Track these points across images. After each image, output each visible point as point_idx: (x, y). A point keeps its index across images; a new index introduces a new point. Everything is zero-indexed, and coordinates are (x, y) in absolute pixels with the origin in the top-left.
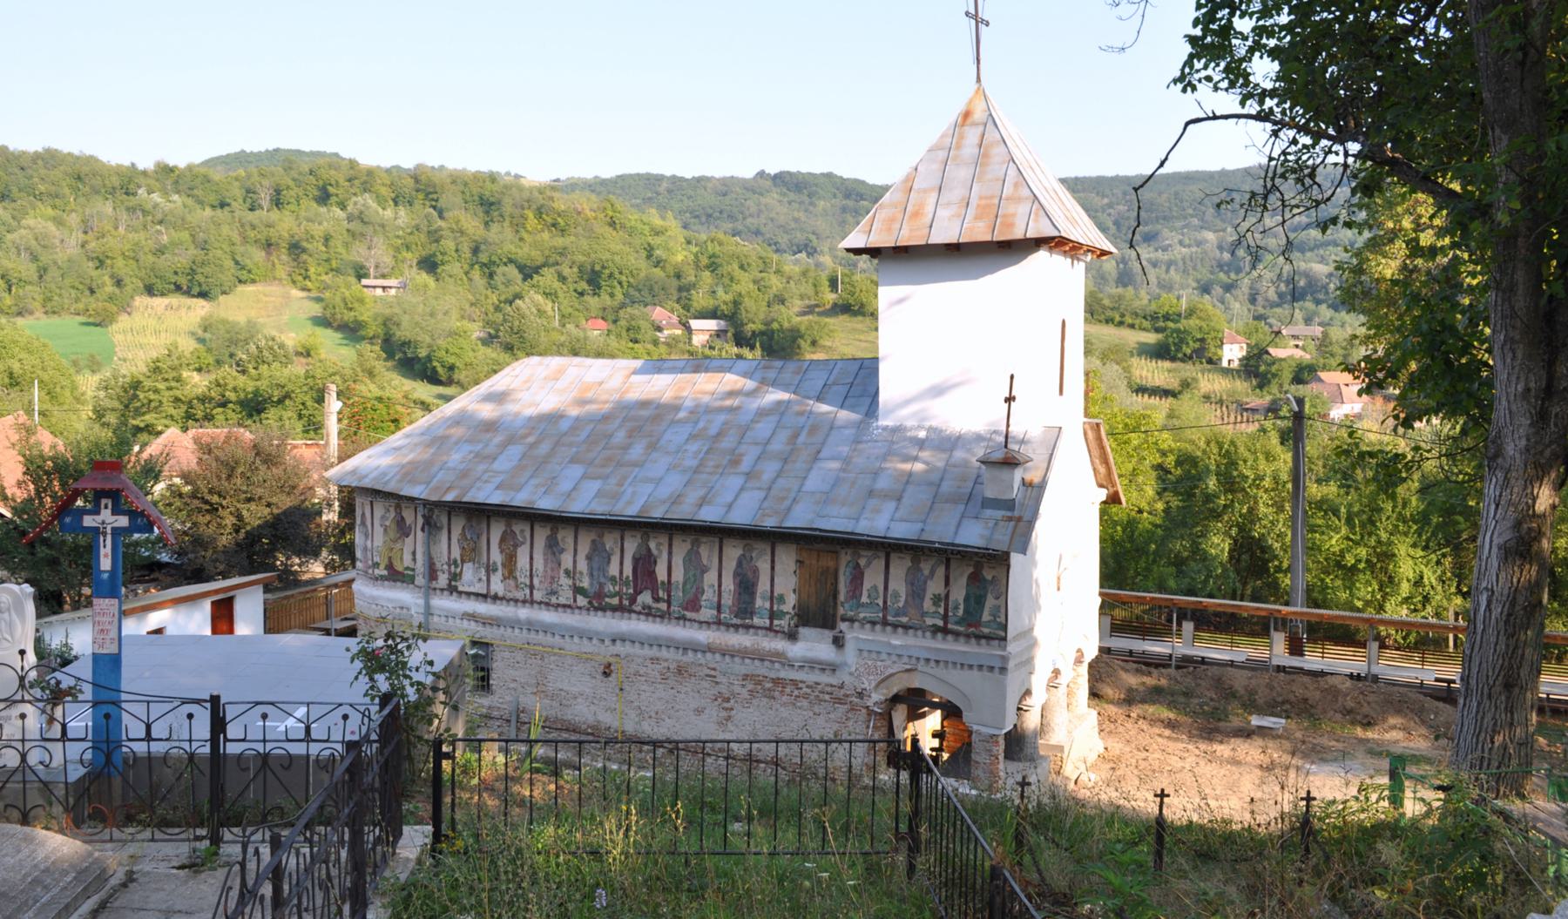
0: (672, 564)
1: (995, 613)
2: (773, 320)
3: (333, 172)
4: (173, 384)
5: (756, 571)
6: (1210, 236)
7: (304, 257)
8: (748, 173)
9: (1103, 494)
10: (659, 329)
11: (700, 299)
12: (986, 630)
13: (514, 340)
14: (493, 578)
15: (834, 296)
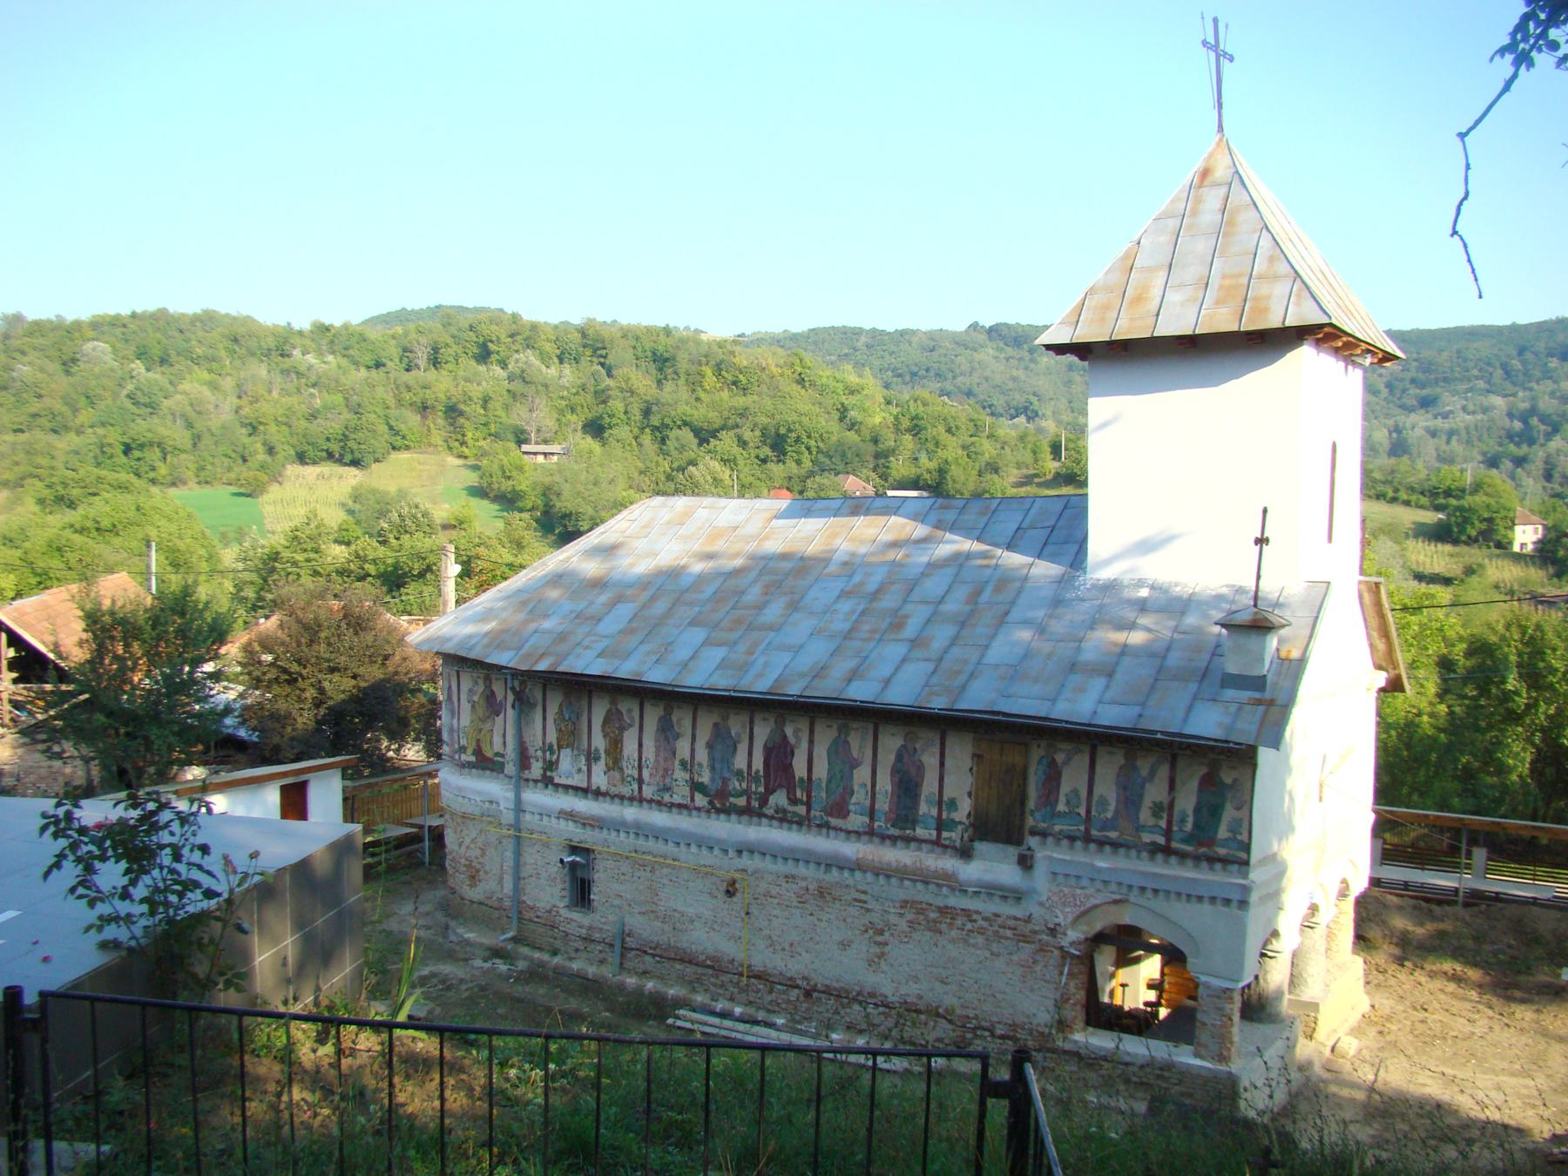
0: (813, 756)
1: (1235, 828)
3: (494, 327)
4: (312, 555)
5: (920, 768)
6: (1498, 401)
7: (462, 420)
8: (958, 325)
9: (1381, 679)
11: (900, 467)
12: (1222, 851)
14: (594, 768)
15: (1056, 464)
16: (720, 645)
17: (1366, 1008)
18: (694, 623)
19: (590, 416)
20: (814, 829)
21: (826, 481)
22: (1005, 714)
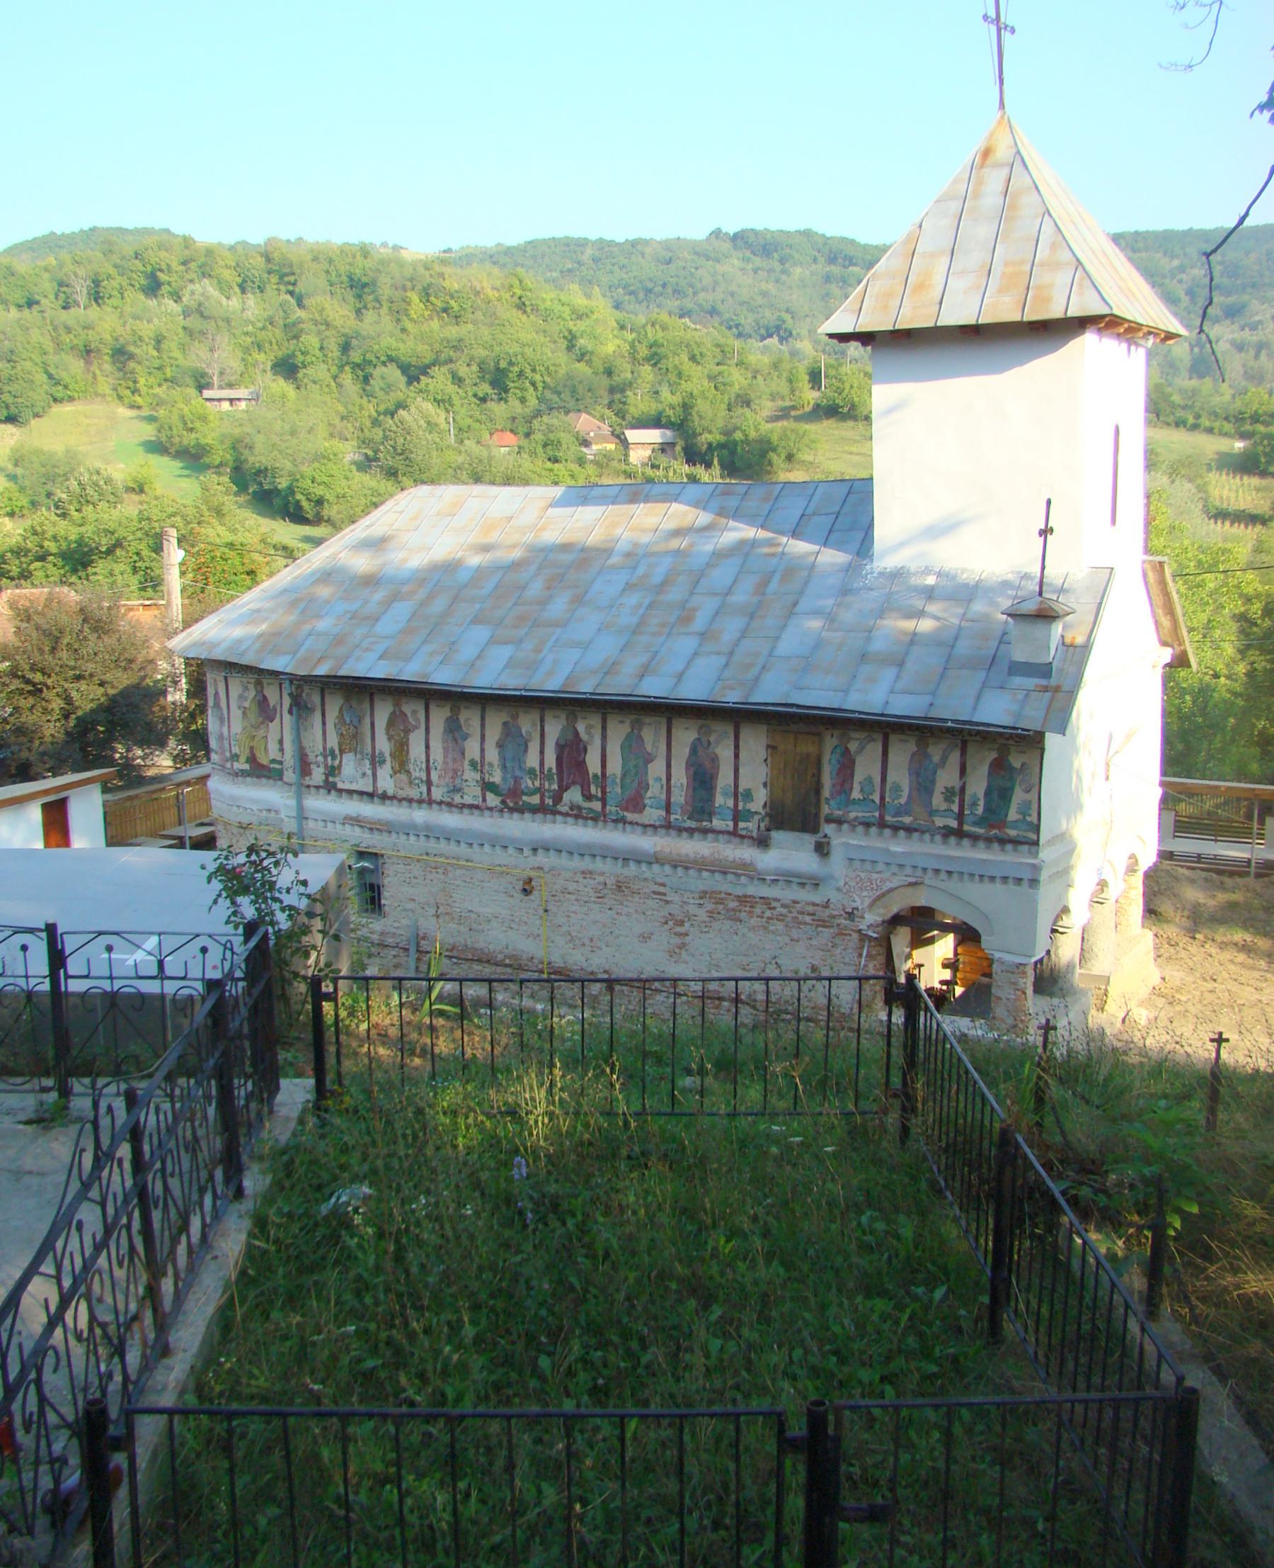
0: (607, 751)
1: (1024, 810)
2: (736, 428)
3: (163, 254)
5: (715, 759)
7: (132, 365)
8: (698, 233)
9: (1166, 655)
10: (586, 443)
11: (639, 403)
12: (1012, 833)
13: (398, 463)
14: (380, 772)
15: (816, 394)
16: (506, 643)
17: (1156, 980)
18: (476, 621)
19: (280, 354)
20: (611, 825)
21: (555, 421)
22: (798, 706)
